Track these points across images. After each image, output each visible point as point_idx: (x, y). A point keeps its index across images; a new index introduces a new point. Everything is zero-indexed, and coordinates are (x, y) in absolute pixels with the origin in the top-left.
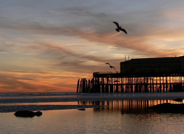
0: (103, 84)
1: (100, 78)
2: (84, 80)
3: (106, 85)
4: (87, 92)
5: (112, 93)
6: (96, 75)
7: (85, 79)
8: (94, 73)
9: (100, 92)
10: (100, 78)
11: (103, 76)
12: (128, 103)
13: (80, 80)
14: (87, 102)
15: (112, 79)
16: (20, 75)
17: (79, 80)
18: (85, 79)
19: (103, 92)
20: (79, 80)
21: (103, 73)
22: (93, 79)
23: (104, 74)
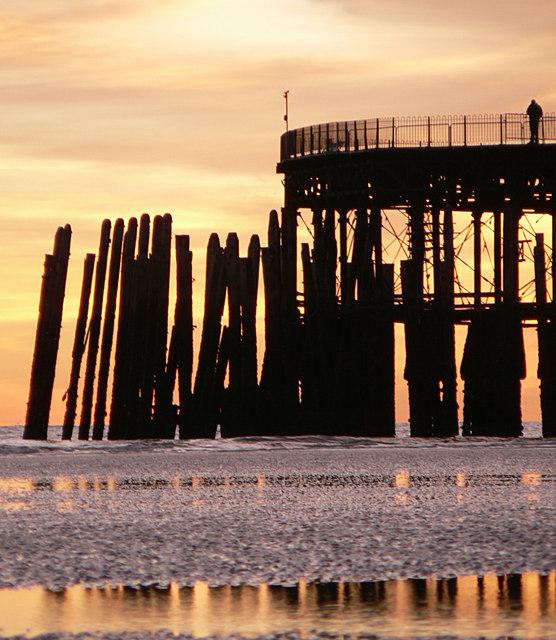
0: (432, 319)
1: (395, 221)
2: (140, 256)
3: (476, 316)
4: (203, 417)
5: (509, 444)
6: (333, 171)
7: (164, 222)
8: (290, 141)
9: (386, 429)
10: (385, 213)
11: (436, 177)
12: (79, 410)
13: (83, 247)
14: (187, 591)
15: (512, 228)
16: (497, 270)
17: (64, 236)
18: (164, 222)
19: (432, 421)
20: (64, 236)
21: (440, 140)
22: (282, 229)
23: (450, 151)
